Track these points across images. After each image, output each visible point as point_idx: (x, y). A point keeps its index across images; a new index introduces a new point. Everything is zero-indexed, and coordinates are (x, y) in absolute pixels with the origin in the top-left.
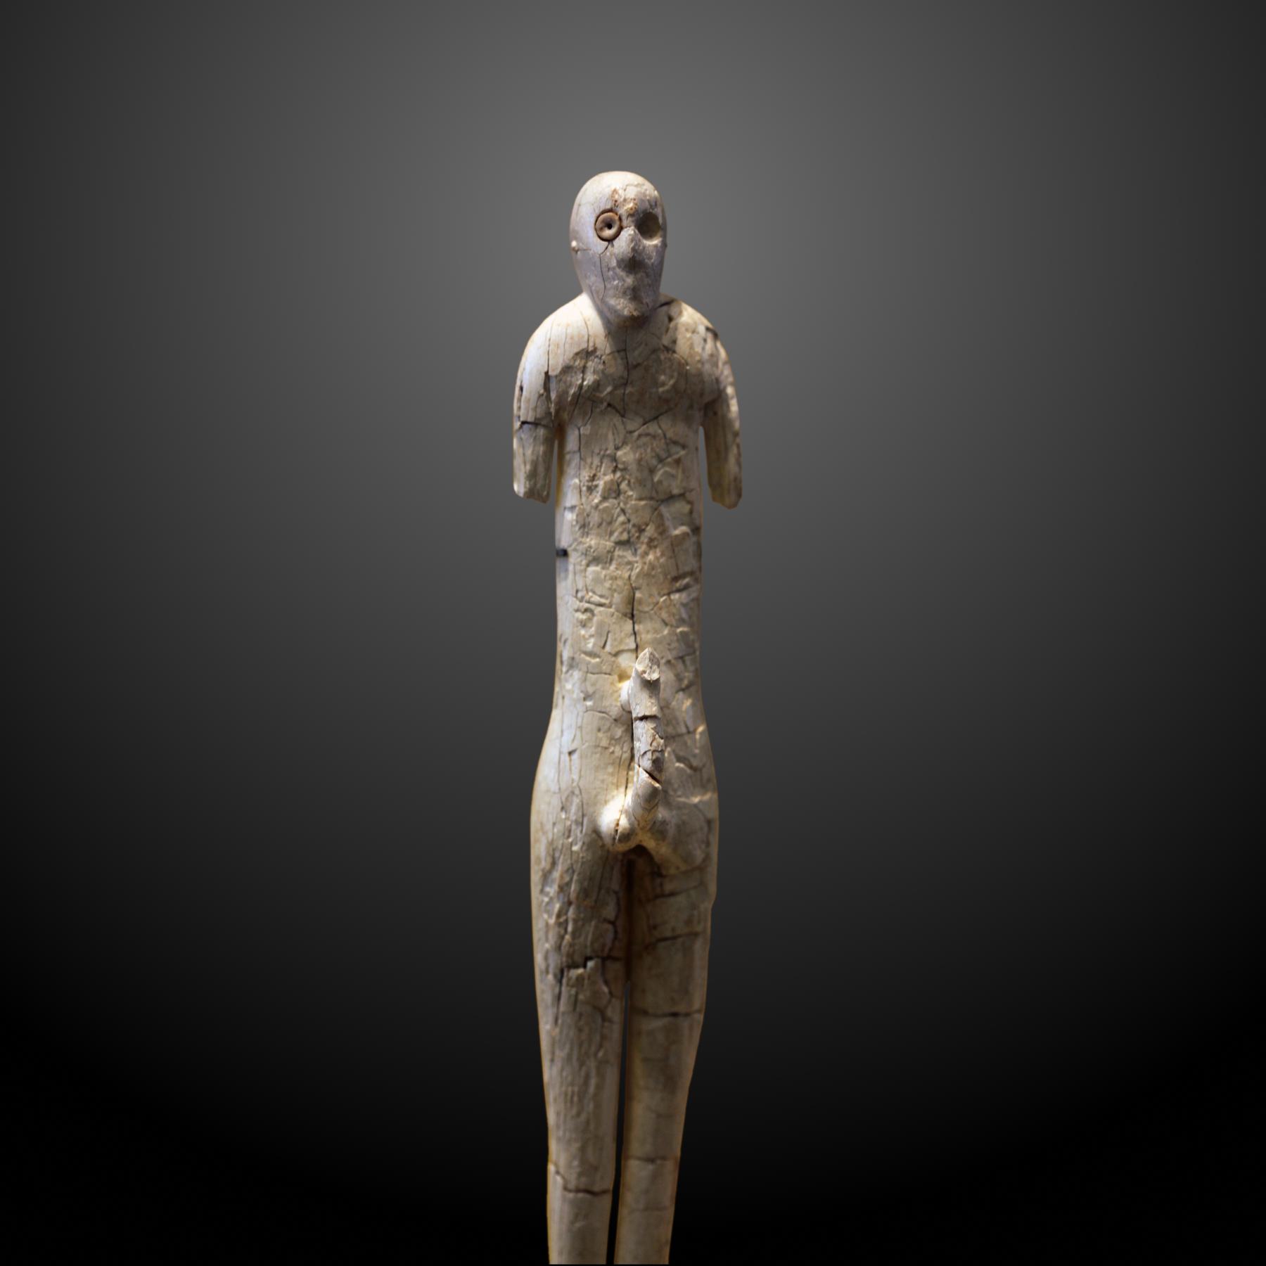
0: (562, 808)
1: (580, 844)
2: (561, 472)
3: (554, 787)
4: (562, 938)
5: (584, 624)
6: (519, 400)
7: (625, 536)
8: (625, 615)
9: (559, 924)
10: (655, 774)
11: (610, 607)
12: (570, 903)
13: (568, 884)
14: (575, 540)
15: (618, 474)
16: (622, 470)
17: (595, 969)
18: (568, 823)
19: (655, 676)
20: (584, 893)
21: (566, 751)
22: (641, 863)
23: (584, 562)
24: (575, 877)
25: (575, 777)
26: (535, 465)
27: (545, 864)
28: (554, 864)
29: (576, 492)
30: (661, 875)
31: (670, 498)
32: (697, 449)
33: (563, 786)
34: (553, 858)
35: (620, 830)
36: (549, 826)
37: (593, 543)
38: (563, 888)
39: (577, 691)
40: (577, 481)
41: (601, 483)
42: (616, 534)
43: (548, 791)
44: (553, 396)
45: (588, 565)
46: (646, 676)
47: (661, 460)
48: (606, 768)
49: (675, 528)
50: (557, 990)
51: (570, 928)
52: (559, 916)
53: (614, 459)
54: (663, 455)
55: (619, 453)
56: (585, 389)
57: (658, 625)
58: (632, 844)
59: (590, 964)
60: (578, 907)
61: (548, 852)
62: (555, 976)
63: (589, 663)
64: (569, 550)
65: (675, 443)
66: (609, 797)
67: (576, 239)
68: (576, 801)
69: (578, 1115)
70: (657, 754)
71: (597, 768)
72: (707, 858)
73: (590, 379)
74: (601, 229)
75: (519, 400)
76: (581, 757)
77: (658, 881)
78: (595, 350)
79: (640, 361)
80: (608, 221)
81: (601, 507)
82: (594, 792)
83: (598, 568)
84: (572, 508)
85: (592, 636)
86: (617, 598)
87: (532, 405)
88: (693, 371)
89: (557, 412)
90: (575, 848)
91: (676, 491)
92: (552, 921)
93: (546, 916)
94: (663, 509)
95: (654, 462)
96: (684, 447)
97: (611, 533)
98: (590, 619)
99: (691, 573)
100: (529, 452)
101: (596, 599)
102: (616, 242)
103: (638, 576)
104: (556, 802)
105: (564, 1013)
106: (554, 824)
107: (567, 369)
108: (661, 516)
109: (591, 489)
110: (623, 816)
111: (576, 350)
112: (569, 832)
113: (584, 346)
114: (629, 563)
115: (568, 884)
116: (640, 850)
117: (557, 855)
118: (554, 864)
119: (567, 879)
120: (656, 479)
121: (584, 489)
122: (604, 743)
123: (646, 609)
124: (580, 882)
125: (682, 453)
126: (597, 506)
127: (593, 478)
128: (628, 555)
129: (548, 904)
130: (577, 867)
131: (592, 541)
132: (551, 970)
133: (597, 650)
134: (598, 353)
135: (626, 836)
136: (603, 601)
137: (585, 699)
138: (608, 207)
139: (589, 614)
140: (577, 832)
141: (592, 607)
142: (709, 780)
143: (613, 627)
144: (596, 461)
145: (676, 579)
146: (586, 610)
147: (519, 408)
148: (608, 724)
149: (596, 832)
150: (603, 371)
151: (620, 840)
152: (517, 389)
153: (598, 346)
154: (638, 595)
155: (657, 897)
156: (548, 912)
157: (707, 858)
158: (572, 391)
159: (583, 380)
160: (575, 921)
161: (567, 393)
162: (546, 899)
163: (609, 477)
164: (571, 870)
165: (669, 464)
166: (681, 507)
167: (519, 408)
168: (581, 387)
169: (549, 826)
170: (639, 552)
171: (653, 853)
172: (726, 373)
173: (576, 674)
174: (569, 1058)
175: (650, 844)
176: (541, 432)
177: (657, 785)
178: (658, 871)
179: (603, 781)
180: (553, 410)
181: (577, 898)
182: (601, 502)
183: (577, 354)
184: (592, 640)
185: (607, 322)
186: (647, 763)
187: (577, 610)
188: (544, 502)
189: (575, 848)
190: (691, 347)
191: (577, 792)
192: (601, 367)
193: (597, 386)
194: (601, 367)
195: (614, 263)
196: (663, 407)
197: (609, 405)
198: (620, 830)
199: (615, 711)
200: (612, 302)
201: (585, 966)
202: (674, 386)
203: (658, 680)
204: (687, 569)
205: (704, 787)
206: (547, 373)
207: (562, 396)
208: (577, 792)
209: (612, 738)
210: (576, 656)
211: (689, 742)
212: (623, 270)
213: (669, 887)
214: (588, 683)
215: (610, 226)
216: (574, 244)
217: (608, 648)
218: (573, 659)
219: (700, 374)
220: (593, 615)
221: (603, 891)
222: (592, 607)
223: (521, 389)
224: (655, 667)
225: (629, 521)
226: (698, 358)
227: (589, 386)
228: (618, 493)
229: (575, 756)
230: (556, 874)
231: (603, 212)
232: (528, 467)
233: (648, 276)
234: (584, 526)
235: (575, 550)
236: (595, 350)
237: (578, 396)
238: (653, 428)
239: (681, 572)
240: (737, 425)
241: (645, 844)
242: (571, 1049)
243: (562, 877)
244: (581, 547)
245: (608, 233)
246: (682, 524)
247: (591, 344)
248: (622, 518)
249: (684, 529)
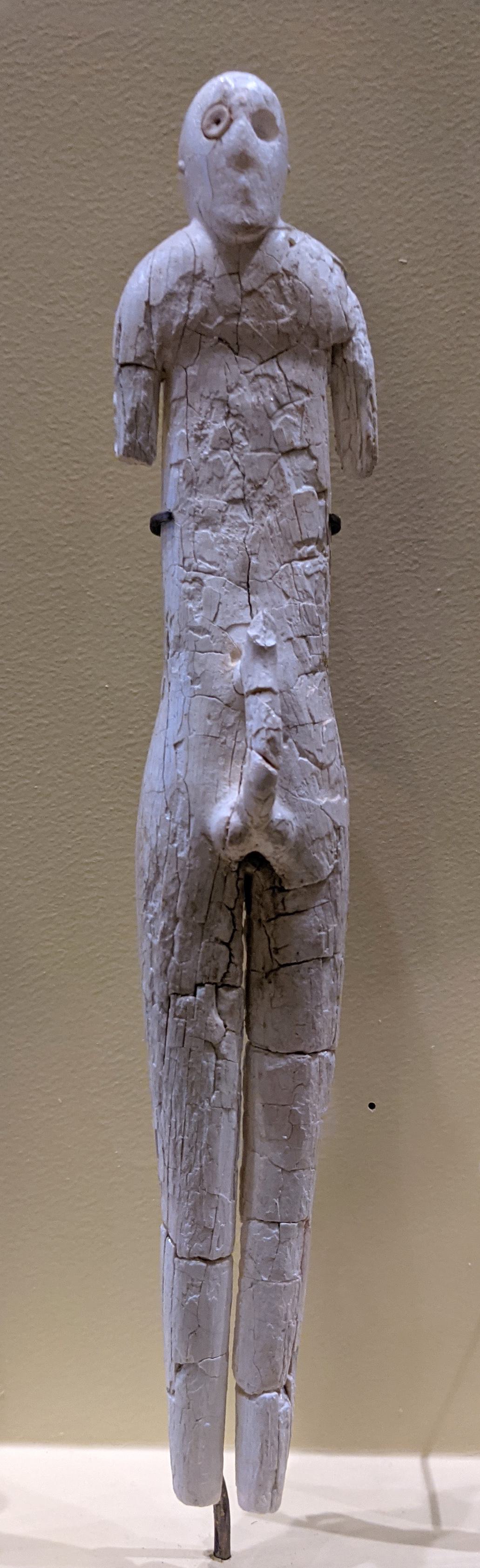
0: (167, 809)
1: (187, 849)
2: (167, 426)
3: (158, 786)
4: (168, 960)
5: (191, 597)
6: (118, 341)
7: (239, 494)
8: (239, 584)
9: (165, 944)
10: (270, 756)
11: (222, 575)
12: (176, 920)
13: (174, 897)
14: (182, 500)
15: (231, 421)
16: (235, 416)
17: (206, 997)
18: (173, 825)
19: (270, 643)
20: (193, 907)
21: (171, 743)
22: (260, 879)
23: (192, 525)
24: (182, 888)
25: (181, 772)
26: (136, 412)
27: (148, 875)
28: (158, 874)
29: (184, 443)
30: (282, 890)
31: (292, 451)
32: (338, 998)
33: (168, 783)
34: (158, 867)
35: (231, 828)
36: (152, 831)
37: (201, 502)
38: (166, 902)
39: (184, 674)
40: (184, 431)
41: (211, 432)
42: (228, 491)
43: (152, 791)
44: (155, 329)
45: (196, 529)
46: (259, 641)
47: (280, 406)
48: (216, 760)
49: (298, 487)
50: (164, 1021)
51: (176, 950)
52: (163, 935)
53: (226, 403)
54: (285, 400)
55: (232, 396)
56: (192, 318)
57: (278, 596)
58: (245, 849)
59: (200, 991)
60: (186, 924)
61: (151, 861)
62: (162, 1005)
63: (197, 640)
64: (175, 514)
65: (297, 387)
66: (219, 794)
67: (183, 158)
68: (182, 799)
69: (190, 1168)
70: (272, 733)
71: (205, 761)
72: (336, 871)
73: (197, 307)
74: (209, 127)
75: (118, 341)
76: (188, 749)
77: (279, 897)
78: (203, 272)
79: (255, 286)
80: (218, 118)
81: (211, 460)
82: (202, 789)
83: (208, 531)
84: (178, 464)
85: (201, 609)
86: (230, 564)
87: (132, 341)
88: (319, 301)
89: (161, 348)
90: (181, 855)
91: (298, 444)
92: (156, 942)
93: (150, 935)
94: (284, 463)
95: (273, 407)
96: (308, 392)
97: (224, 490)
98: (198, 590)
99: (317, 541)
100: (129, 399)
101: (205, 566)
102: (225, 139)
103: (254, 539)
104: (160, 803)
105: (171, 1049)
106: (158, 827)
107: (170, 296)
108: (280, 470)
109: (199, 439)
110: (235, 813)
111: (181, 274)
112: (173, 836)
113: (190, 268)
114: (243, 525)
115: (174, 897)
116: (256, 859)
117: (161, 864)
118: (158, 874)
119: (173, 890)
120: (274, 428)
121: (192, 439)
122: (215, 732)
123: (264, 578)
124: (188, 894)
125: (306, 399)
126: (205, 460)
127: (201, 427)
128: (241, 513)
129: (152, 922)
130: (183, 877)
131: (200, 500)
132: (156, 999)
133: (206, 625)
134: (207, 276)
135: (239, 837)
136: (213, 568)
137: (192, 682)
138: (217, 100)
139: (196, 584)
140: (182, 833)
141: (201, 575)
142: (338, 782)
143: (224, 598)
144: (206, 406)
145: (299, 544)
146: (194, 579)
147: (118, 350)
148: (219, 709)
149: (205, 835)
150: (212, 297)
151: (231, 842)
152: (116, 328)
153: (206, 267)
154: (254, 561)
155: (278, 915)
156: (152, 931)
157: (336, 871)
158: (176, 322)
159: (189, 308)
160: (183, 941)
161: (171, 324)
162: (151, 916)
163: (218, 426)
164: (176, 879)
165: (290, 411)
166: (302, 462)
167: (118, 350)
168: (186, 316)
169: (152, 831)
170: (256, 511)
171: (273, 862)
172: (358, 320)
173: (184, 655)
174: (177, 1103)
175: (267, 849)
176: (143, 374)
177: (271, 769)
178: (278, 886)
179: (213, 776)
180: (154, 348)
181: (184, 913)
182: (210, 454)
183: (183, 278)
184: (202, 613)
185: (217, 240)
186: (260, 743)
187: (184, 581)
188: (149, 462)
189: (181, 855)
190: (316, 274)
191: (183, 789)
192: (210, 292)
193: (205, 315)
194: (210, 292)
195: (223, 162)
196: (283, 344)
197: (220, 339)
198: (231, 828)
199: (226, 694)
200: (221, 210)
201: (195, 995)
202: (295, 318)
203: (273, 647)
204: (312, 534)
205: (332, 787)
206: (147, 303)
207: (164, 329)
208: (183, 789)
209: (223, 727)
210: (183, 634)
211: (313, 734)
212: (235, 169)
213: (291, 906)
214: (196, 664)
215: (218, 122)
216: (181, 163)
217: (218, 622)
218: (180, 637)
219: (325, 306)
220: (202, 584)
221: (213, 906)
222: (201, 575)
223: (120, 326)
224: (270, 632)
225: (244, 475)
226: (324, 287)
227: (195, 316)
228: (232, 443)
229: (181, 749)
230: (160, 886)
231: (212, 106)
232: (128, 417)
233: (262, 178)
234: (192, 484)
235: (182, 512)
236: (203, 272)
237: (184, 328)
238: (272, 368)
239: (305, 537)
240: (371, 373)
241: (261, 850)
242: (180, 1090)
243: (166, 888)
244: (188, 509)
245: (215, 130)
246: (307, 484)
247: (198, 266)
248: (236, 472)
249: (310, 488)
